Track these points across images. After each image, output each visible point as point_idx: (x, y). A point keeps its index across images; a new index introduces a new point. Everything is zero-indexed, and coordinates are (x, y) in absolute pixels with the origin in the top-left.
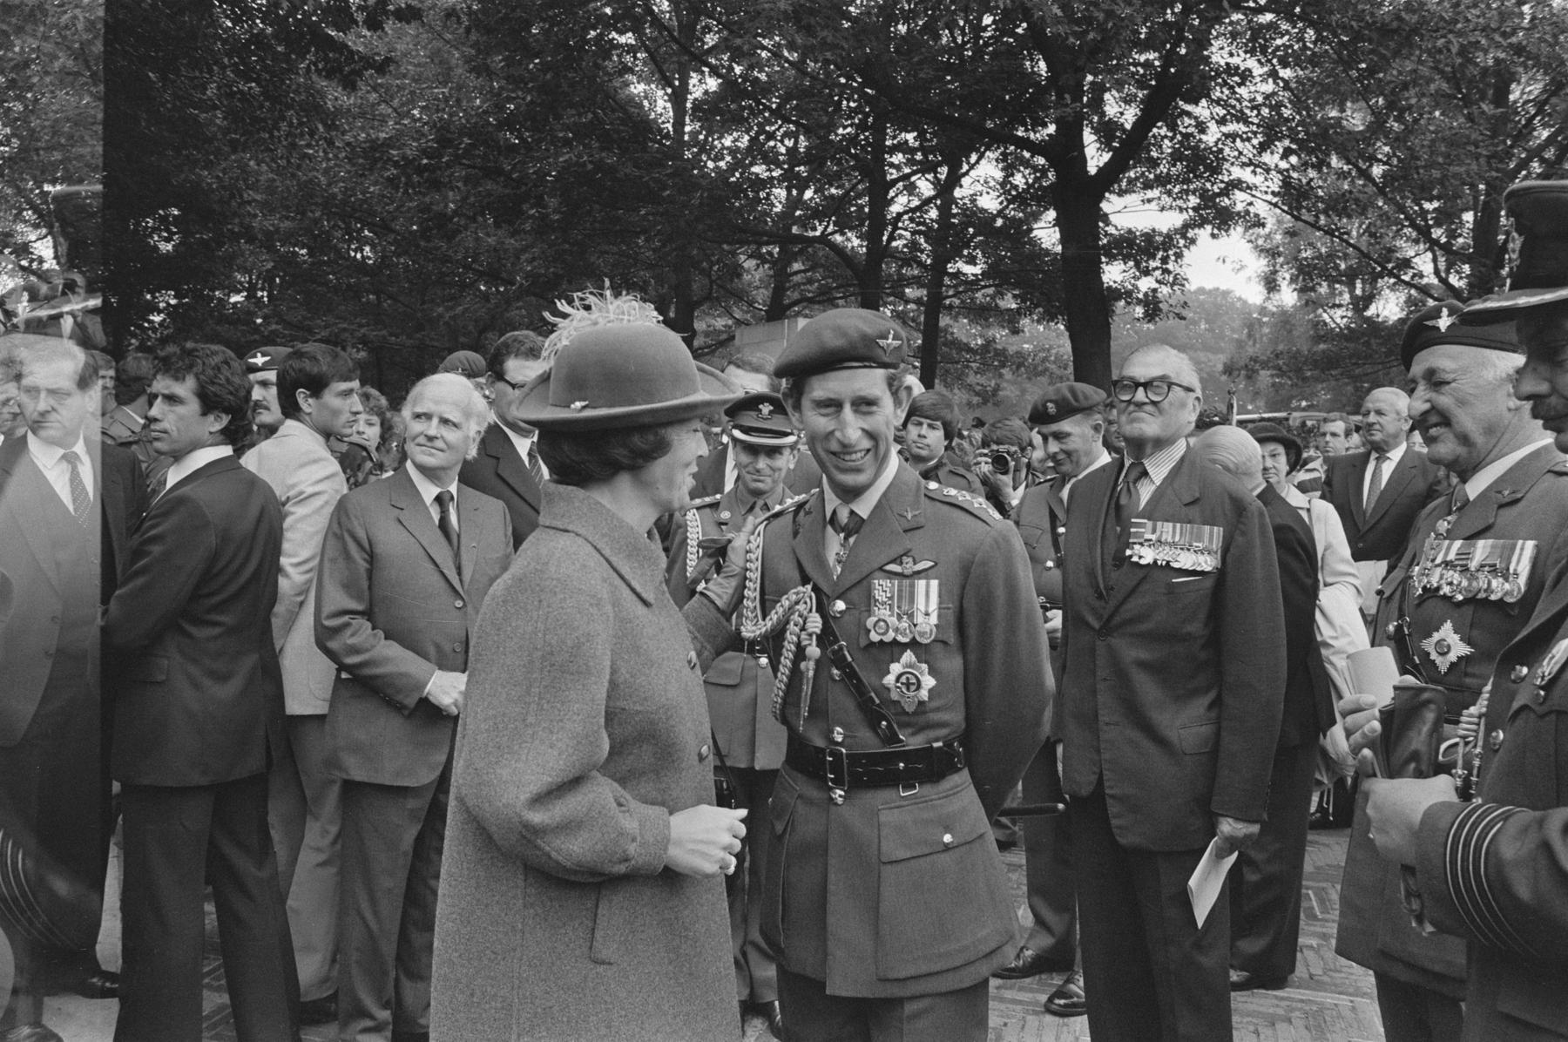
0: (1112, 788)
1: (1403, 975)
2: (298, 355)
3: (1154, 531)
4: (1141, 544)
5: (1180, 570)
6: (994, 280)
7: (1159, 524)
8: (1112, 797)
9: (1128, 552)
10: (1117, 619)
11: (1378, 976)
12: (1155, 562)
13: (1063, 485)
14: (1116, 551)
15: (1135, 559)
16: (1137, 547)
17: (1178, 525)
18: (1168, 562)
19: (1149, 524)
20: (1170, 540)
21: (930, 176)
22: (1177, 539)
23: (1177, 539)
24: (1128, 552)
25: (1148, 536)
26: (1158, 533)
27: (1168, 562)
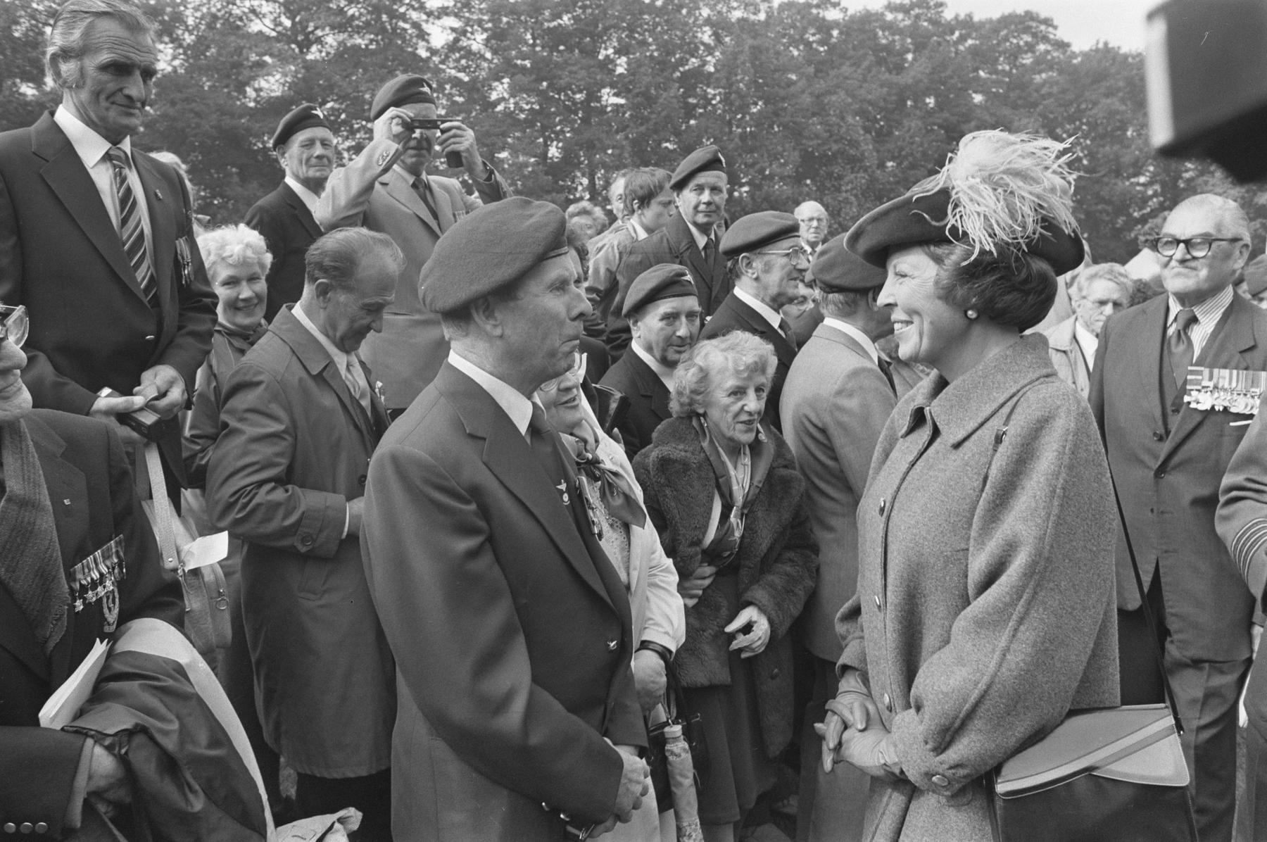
0: (1171, 607)
1: (312, 121)
2: (153, 42)
3: (1211, 378)
4: (1199, 391)
5: (1237, 414)
6: (377, 35)
7: (1216, 371)
8: (1173, 615)
9: (1186, 399)
10: (1176, 460)
11: (1141, 606)
12: (1213, 407)
13: (383, 80)
14: (1176, 398)
15: (1193, 405)
16: (1194, 393)
17: (1235, 372)
18: (1225, 408)
19: (1206, 371)
20: (1226, 386)
21: (346, 9)
22: (1234, 385)
23: (1234, 385)
24: (1186, 399)
25: (1205, 383)
26: (1215, 380)
27: (1225, 408)
